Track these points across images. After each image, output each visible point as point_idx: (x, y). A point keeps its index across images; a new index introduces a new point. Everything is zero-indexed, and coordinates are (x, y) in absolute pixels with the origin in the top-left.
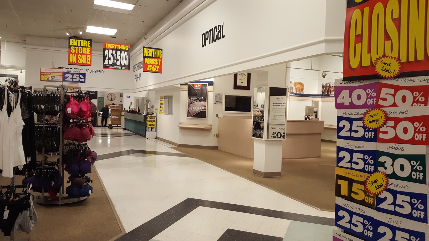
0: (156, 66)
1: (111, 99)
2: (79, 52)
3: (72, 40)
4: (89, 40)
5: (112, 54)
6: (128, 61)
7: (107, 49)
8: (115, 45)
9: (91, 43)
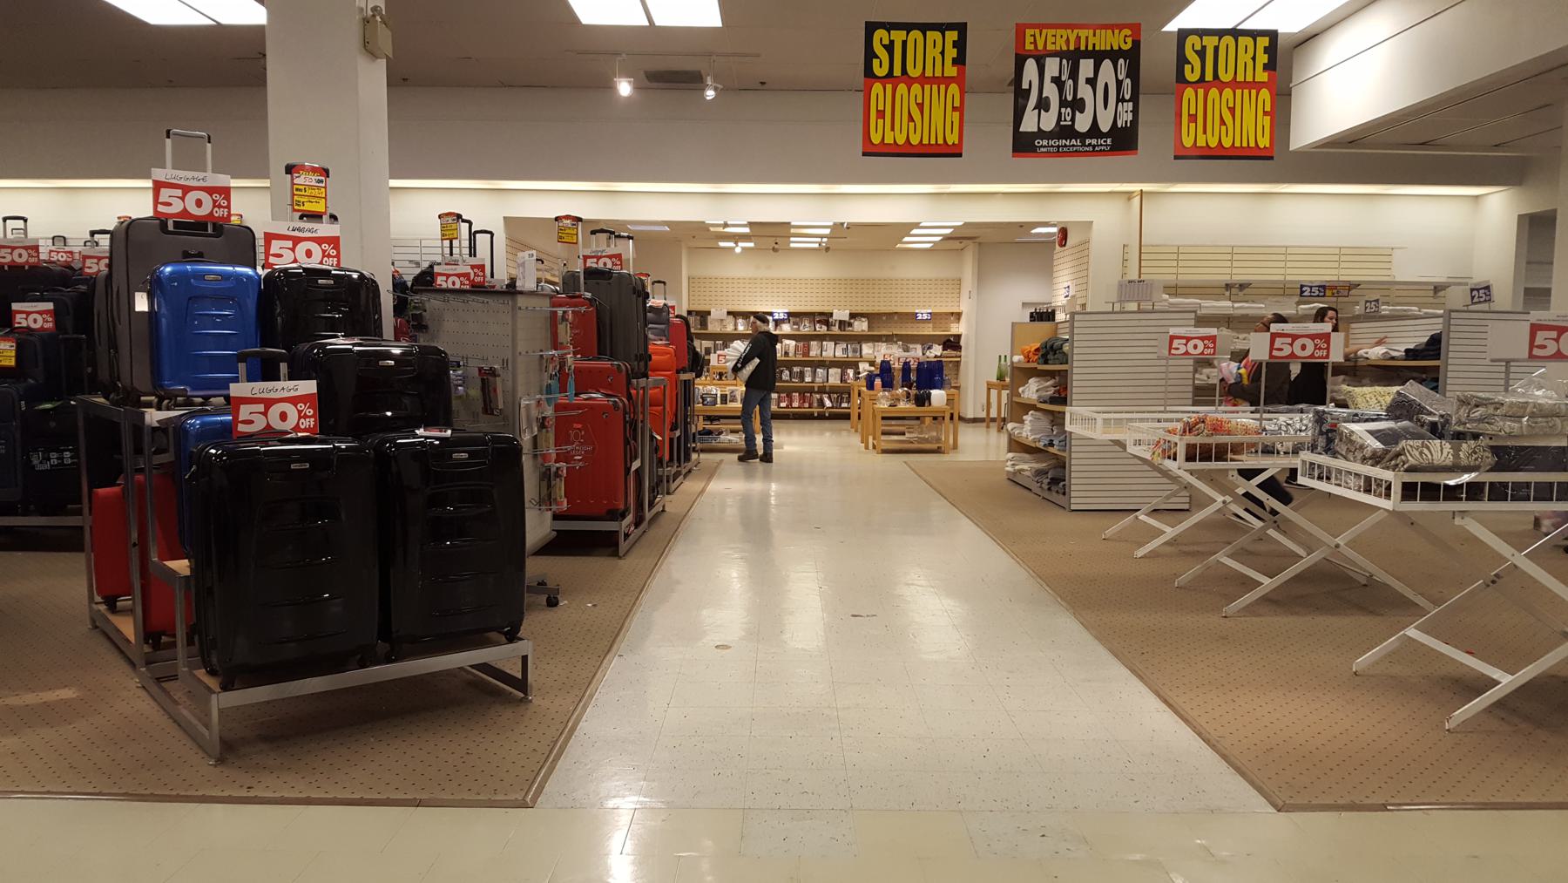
5: (1057, 81)
7: (1030, 57)
8: (1069, 31)
9: (960, 45)
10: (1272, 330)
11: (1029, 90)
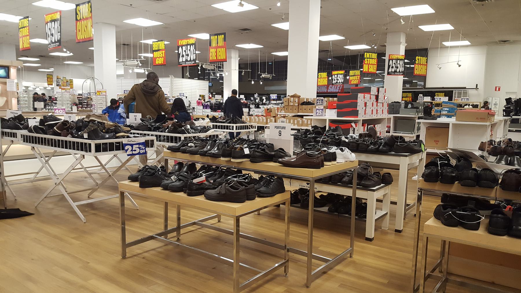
2: (370, 63)
3: (366, 53)
5: (336, 77)
10: (317, 108)
11: (390, 65)
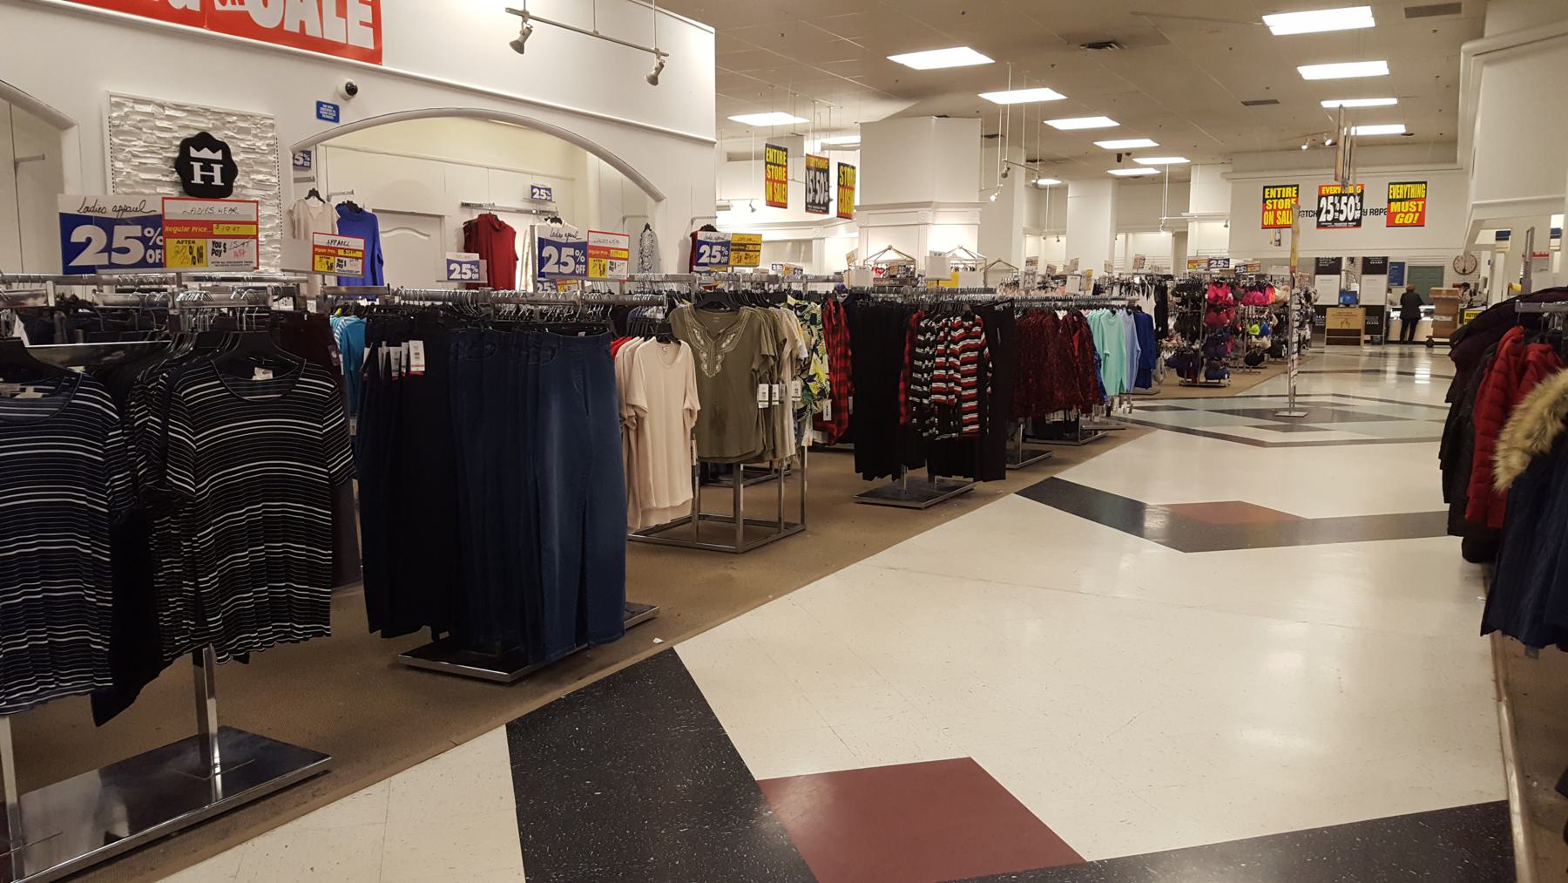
0: (1412, 215)
1: (1464, 270)
2: (1279, 207)
4: (1295, 186)
5: (1333, 204)
6: (1359, 212)
9: (1297, 190)
